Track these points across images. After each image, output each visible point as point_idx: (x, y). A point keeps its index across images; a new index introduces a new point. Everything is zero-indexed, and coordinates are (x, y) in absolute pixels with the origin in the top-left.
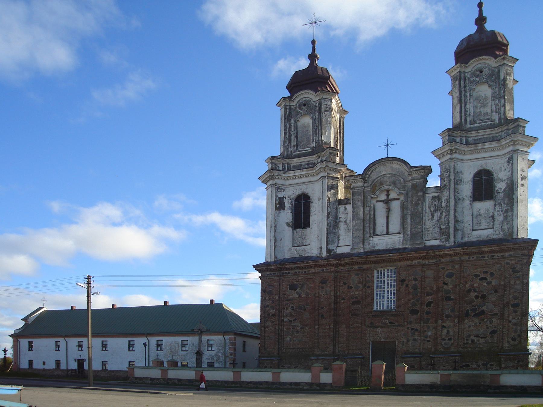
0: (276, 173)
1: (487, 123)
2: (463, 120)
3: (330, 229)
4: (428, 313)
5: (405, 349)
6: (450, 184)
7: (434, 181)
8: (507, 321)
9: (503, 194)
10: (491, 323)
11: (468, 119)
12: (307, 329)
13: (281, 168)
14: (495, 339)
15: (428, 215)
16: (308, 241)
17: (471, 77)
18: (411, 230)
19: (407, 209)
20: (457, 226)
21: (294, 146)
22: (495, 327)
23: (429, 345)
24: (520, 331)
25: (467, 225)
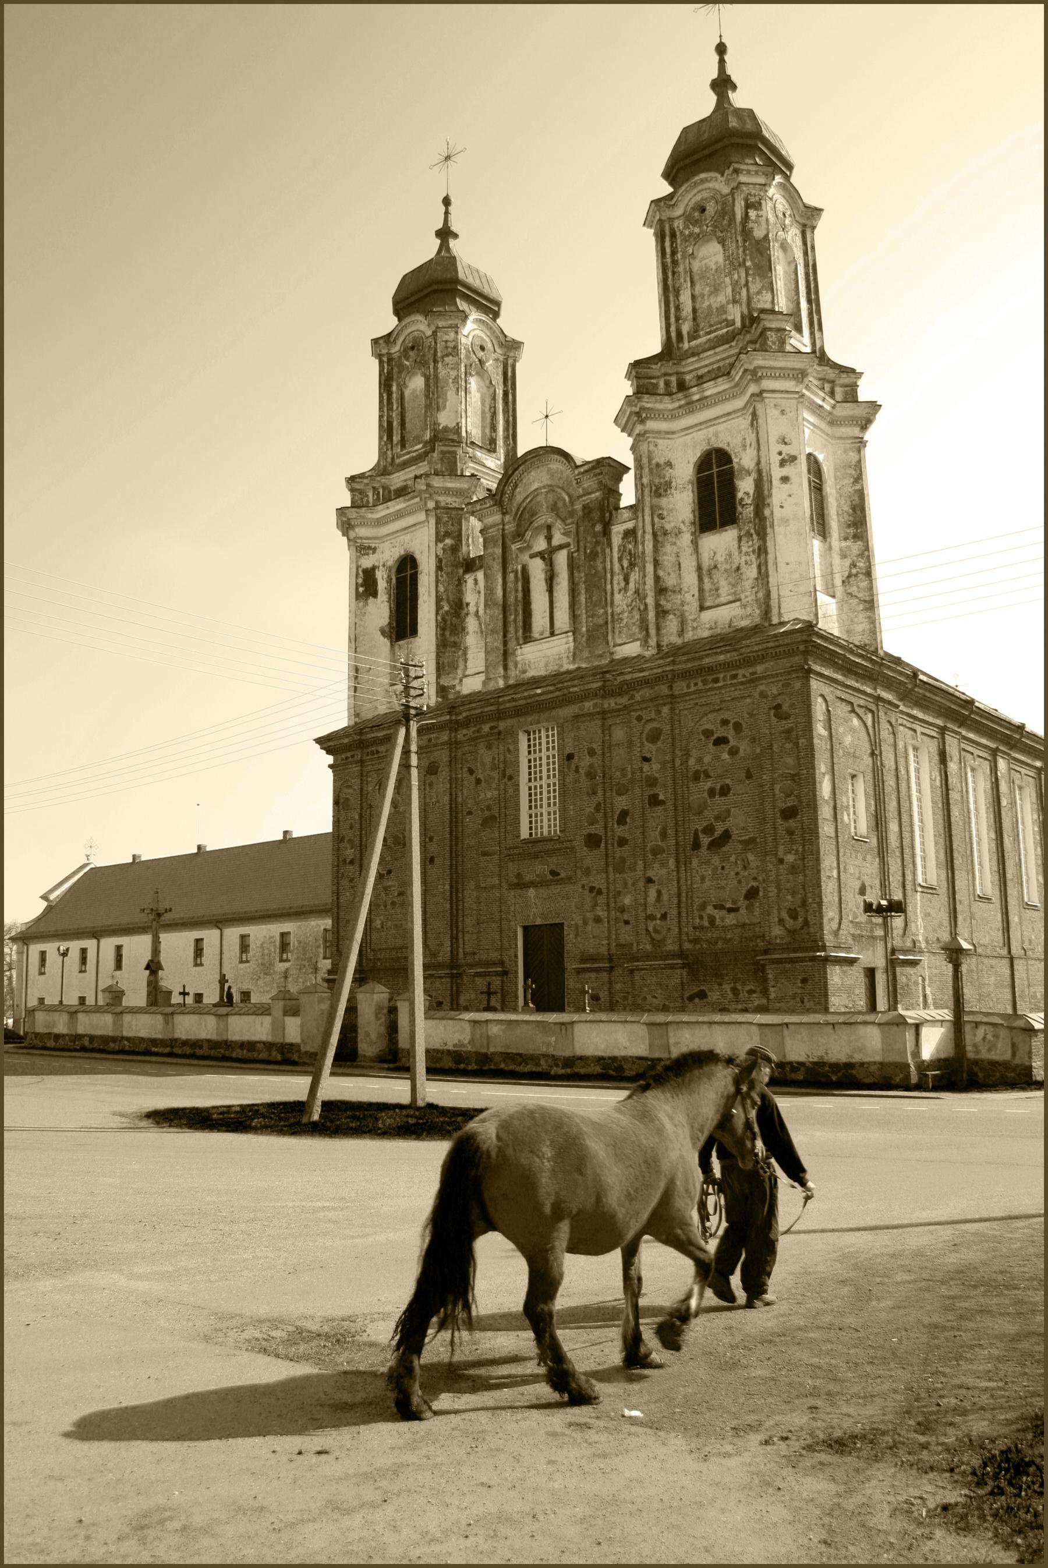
1: (720, 332)
2: (673, 335)
4: (622, 842)
7: (628, 492)
11: (685, 328)
15: (618, 579)
17: (686, 227)
22: (755, 879)
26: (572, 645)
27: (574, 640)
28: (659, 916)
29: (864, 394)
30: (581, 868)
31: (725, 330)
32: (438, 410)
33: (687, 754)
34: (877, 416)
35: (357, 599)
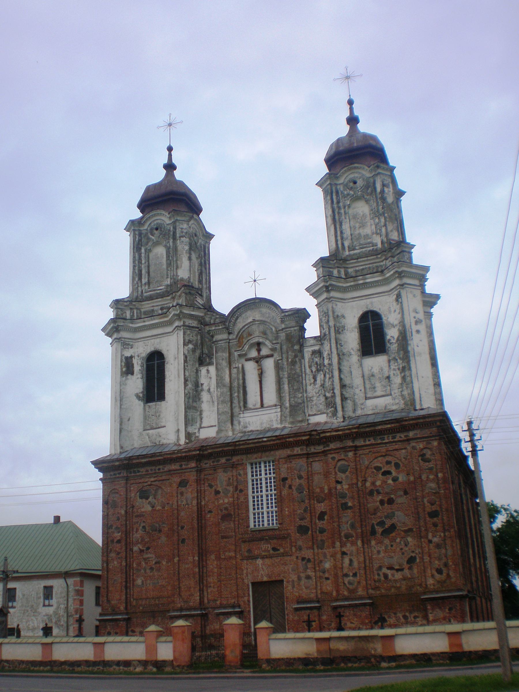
0: (121, 323)
1: (369, 249)
2: (340, 246)
3: (188, 402)
4: (322, 531)
5: (297, 594)
6: (329, 333)
7: (312, 328)
8: (426, 541)
9: (396, 345)
10: (406, 545)
11: (346, 244)
12: (164, 563)
13: (128, 317)
14: (415, 571)
15: (309, 379)
16: (164, 420)
18: (289, 400)
19: (282, 369)
20: (344, 393)
21: (145, 284)
22: (413, 552)
23: (328, 586)
24: (446, 556)
25: (359, 393)
26: (279, 414)
27: (281, 411)
28: (351, 574)
29: (430, 288)
30: (295, 546)
31: (371, 248)
32: (177, 268)
33: (365, 481)
34: (438, 302)
35: (121, 375)
